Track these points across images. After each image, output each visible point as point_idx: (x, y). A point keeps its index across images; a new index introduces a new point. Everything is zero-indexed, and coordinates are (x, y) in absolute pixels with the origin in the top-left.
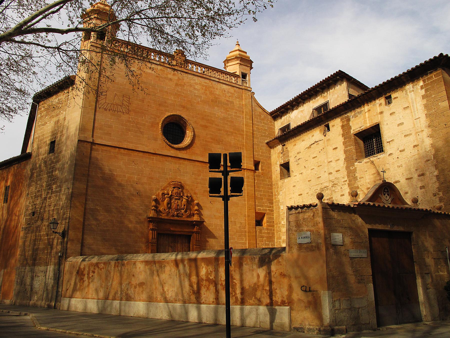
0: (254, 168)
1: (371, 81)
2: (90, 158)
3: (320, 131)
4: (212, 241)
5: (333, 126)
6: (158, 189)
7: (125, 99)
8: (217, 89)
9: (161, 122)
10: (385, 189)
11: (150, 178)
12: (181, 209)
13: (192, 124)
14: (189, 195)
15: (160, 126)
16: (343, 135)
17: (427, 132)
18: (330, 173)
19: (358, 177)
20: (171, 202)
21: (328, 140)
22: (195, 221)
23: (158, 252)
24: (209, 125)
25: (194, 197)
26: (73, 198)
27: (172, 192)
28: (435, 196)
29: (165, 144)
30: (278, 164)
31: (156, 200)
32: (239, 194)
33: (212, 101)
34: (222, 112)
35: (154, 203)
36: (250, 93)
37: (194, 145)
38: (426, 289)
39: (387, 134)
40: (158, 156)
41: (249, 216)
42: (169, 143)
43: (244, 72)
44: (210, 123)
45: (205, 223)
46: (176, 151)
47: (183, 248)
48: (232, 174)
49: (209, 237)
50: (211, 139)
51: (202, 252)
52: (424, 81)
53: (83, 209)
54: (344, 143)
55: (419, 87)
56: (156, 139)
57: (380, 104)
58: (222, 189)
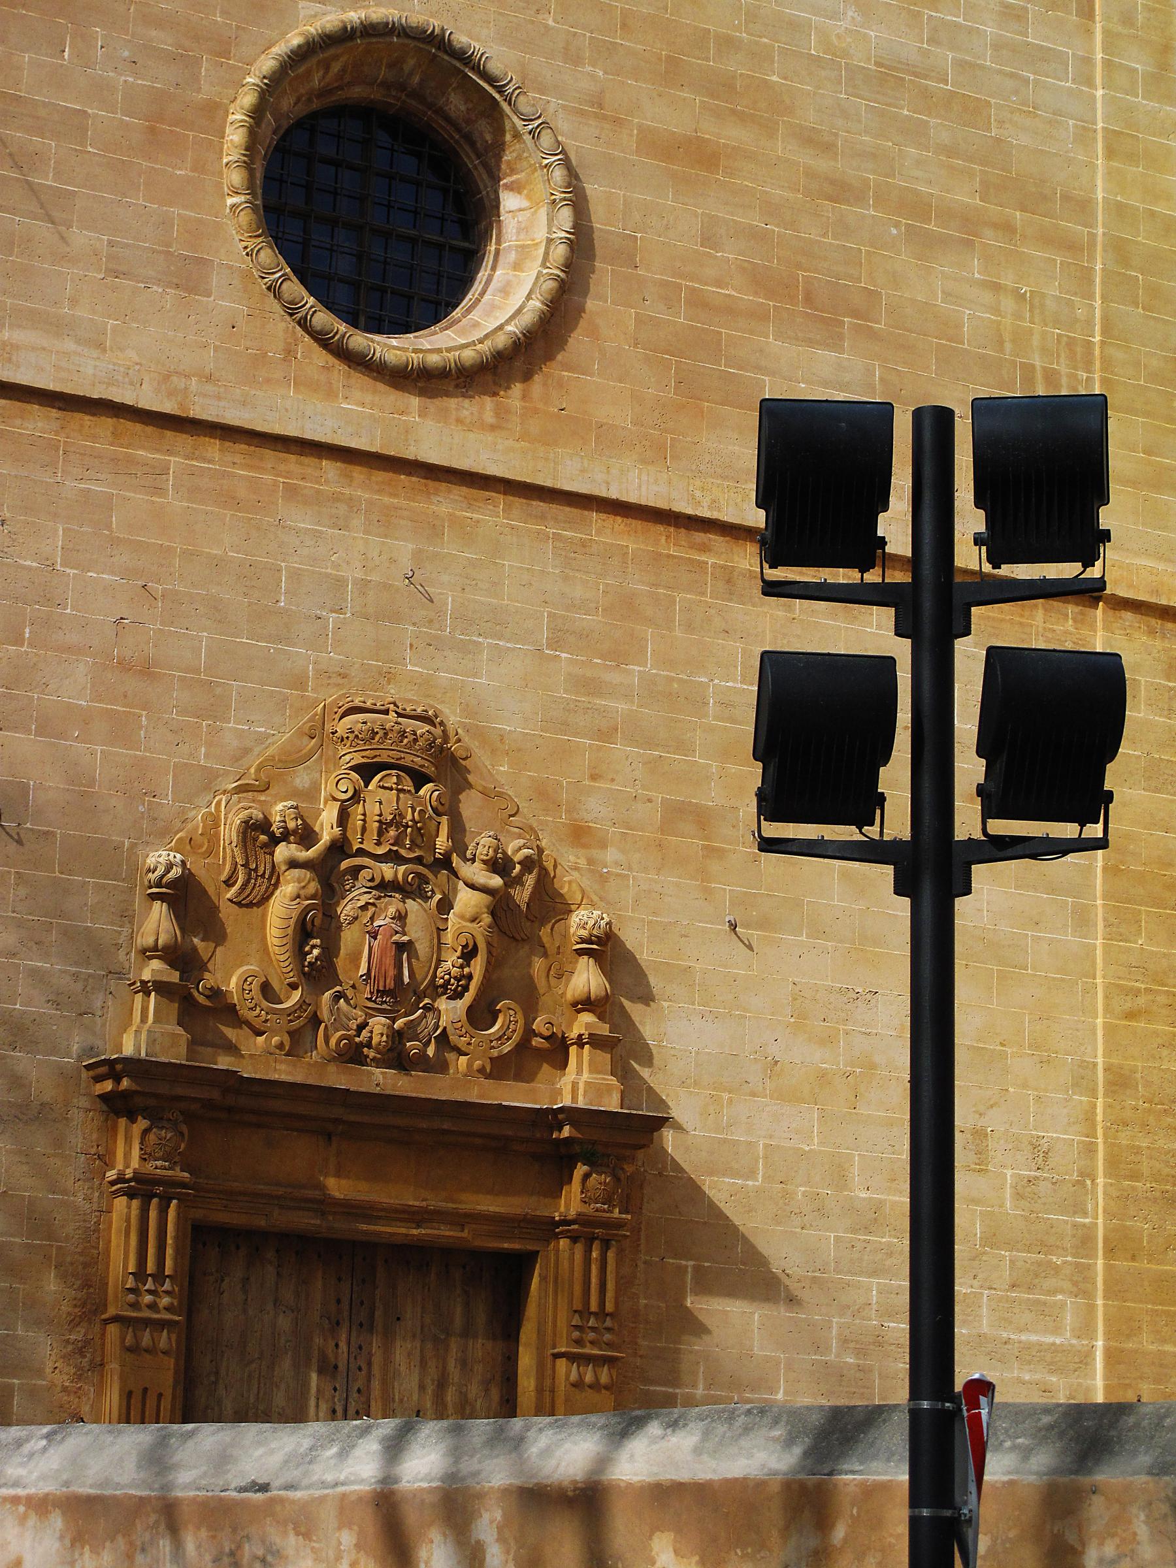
4: (734, 1325)
6: (208, 782)
9: (248, 99)
11: (124, 666)
12: (437, 990)
13: (563, 124)
14: (517, 849)
15: (235, 137)
20: (330, 914)
22: (572, 1115)
23: (190, 1410)
24: (733, 134)
25: (571, 871)
27: (343, 818)
29: (281, 326)
31: (183, 895)
32: (1068, 830)
35: (157, 924)
37: (578, 342)
40: (213, 448)
41: (1119, 1081)
42: (322, 318)
44: (741, 118)
45: (669, 1139)
46: (391, 398)
47: (442, 1384)
48: (992, 628)
49: (706, 1284)
50: (759, 280)
51: (654, 1428)
56: (189, 277)
58: (896, 779)
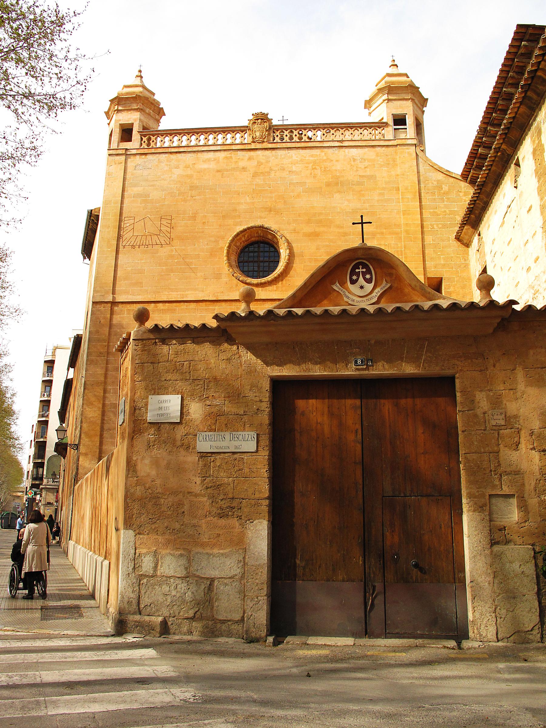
2: (111, 326)
7: (164, 222)
8: (337, 161)
24: (322, 229)
26: (86, 391)
29: (235, 281)
33: (328, 185)
34: (348, 201)
37: (292, 273)
38: (496, 536)
43: (399, 112)
53: (101, 406)
56: (218, 276)
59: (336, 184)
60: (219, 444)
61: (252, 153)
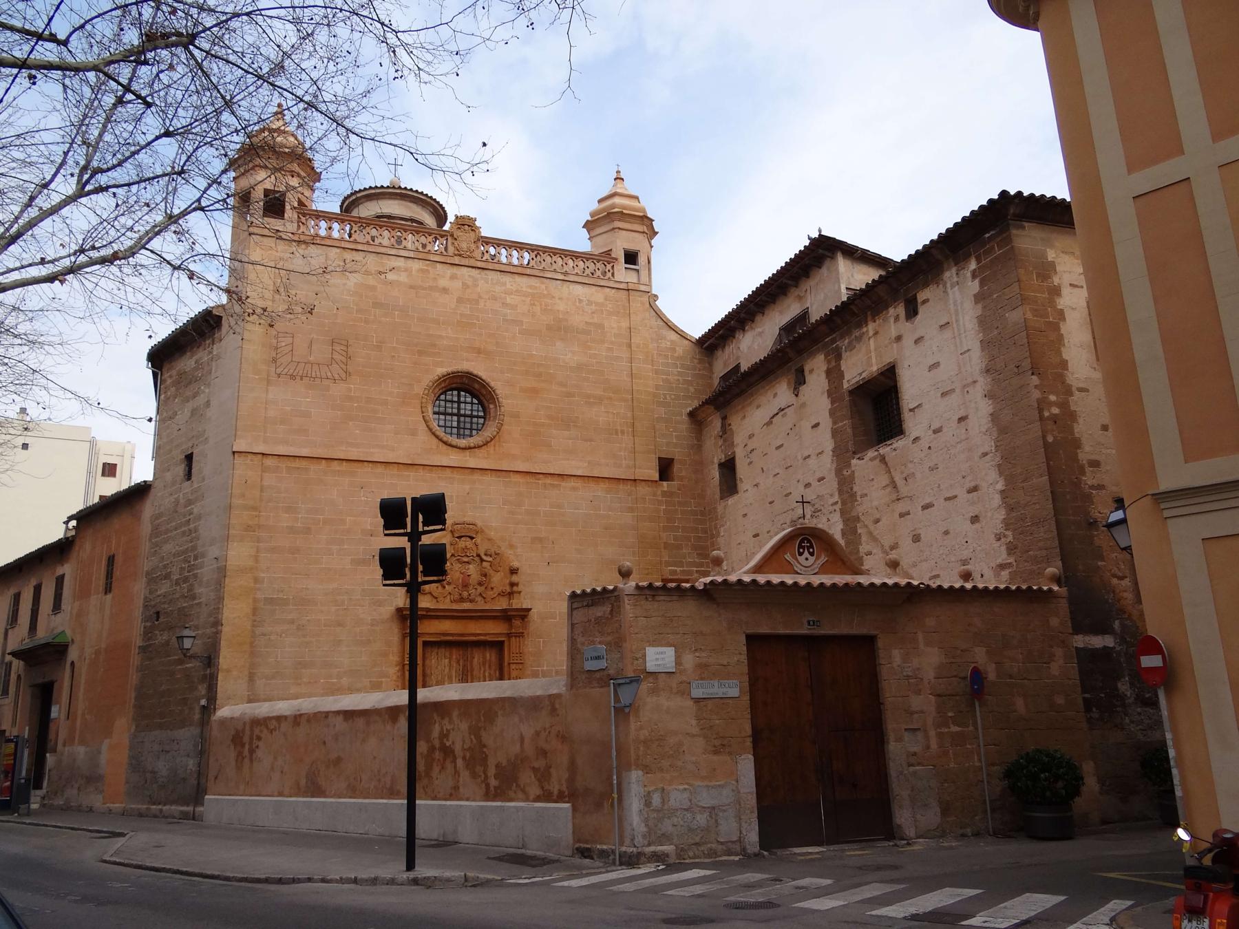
0: (656, 476)
1: (898, 250)
3: (789, 384)
5: (811, 371)
7: (337, 348)
10: (802, 541)
16: (830, 393)
17: (983, 384)
18: (808, 485)
19: (859, 494)
21: (803, 405)
28: (999, 539)
30: (716, 461)
33: (549, 328)
36: (645, 299)
39: (912, 389)
43: (632, 247)
52: (978, 260)
54: (832, 413)
55: (969, 275)
57: (897, 318)
59: (559, 329)
60: (711, 691)
61: (455, 270)
